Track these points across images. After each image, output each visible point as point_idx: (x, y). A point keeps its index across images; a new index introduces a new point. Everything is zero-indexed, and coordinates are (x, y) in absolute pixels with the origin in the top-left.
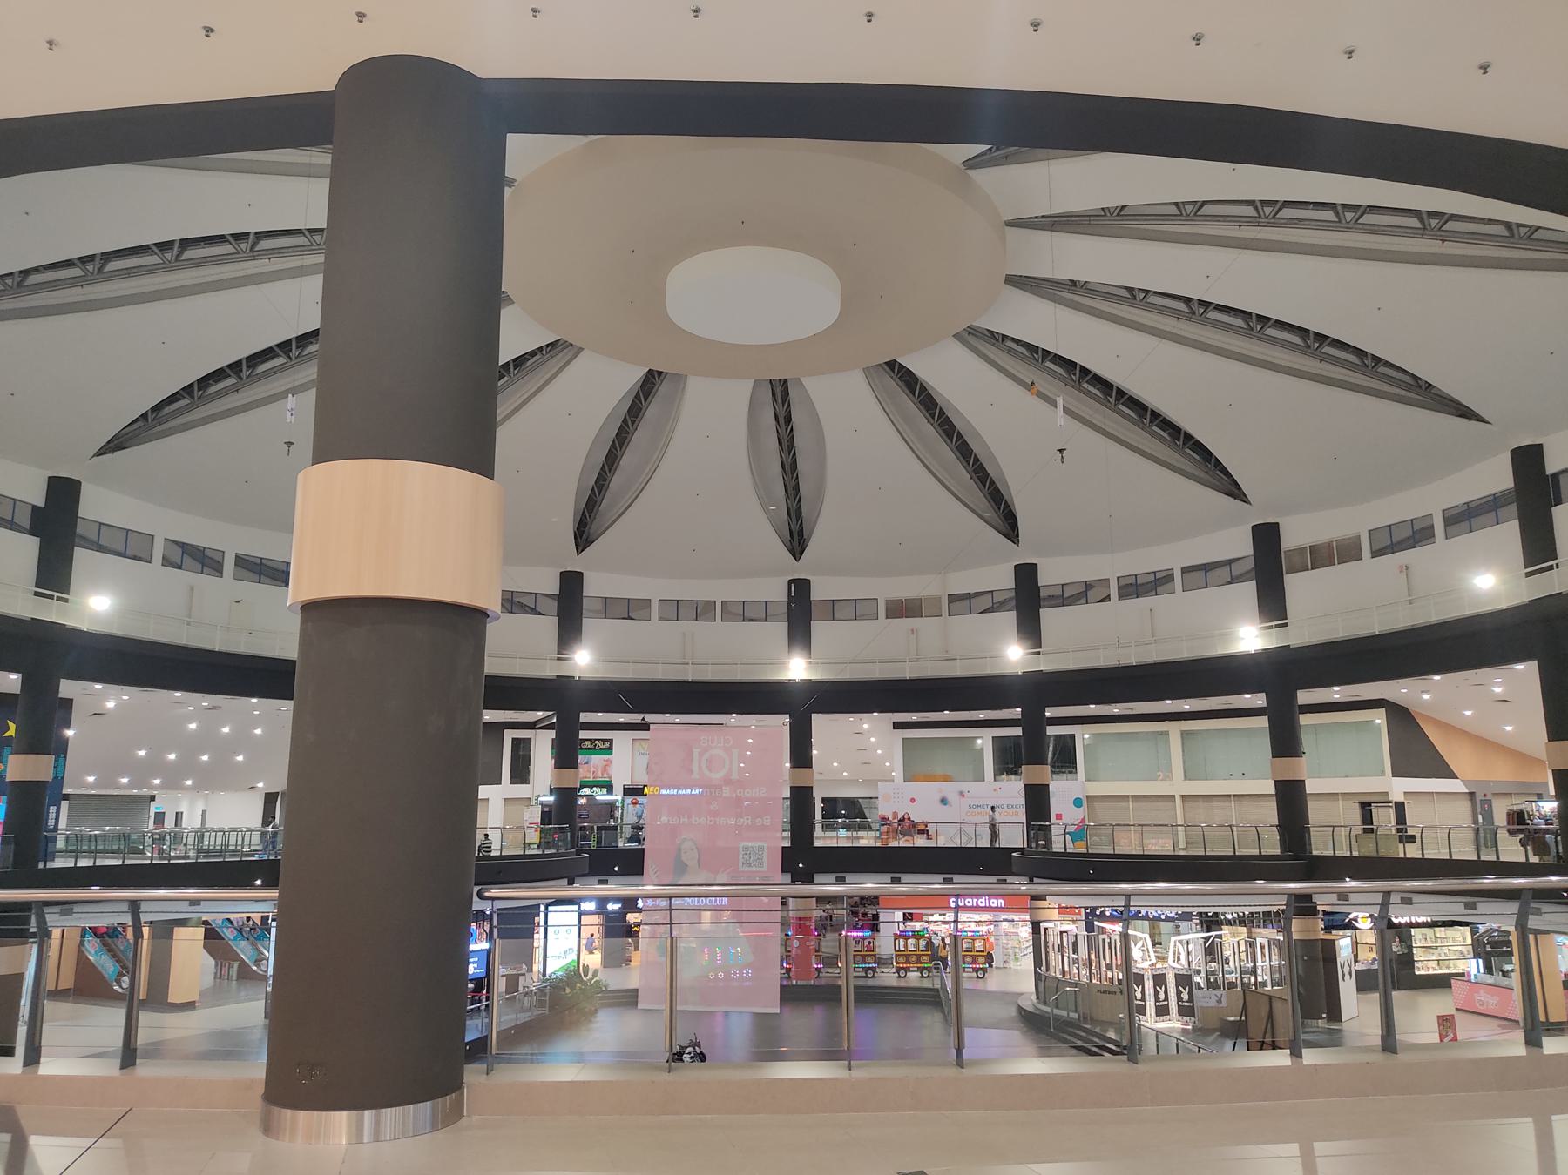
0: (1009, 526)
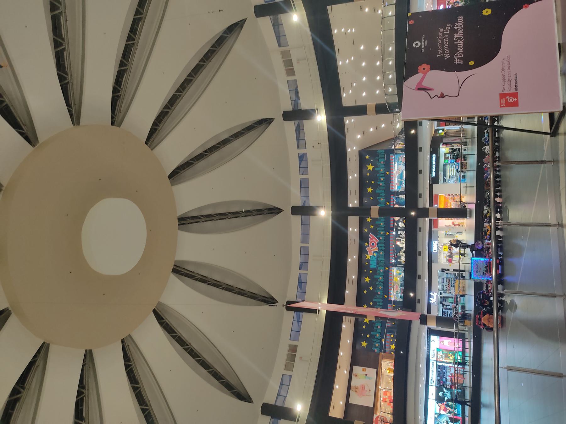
0: (266, 122)
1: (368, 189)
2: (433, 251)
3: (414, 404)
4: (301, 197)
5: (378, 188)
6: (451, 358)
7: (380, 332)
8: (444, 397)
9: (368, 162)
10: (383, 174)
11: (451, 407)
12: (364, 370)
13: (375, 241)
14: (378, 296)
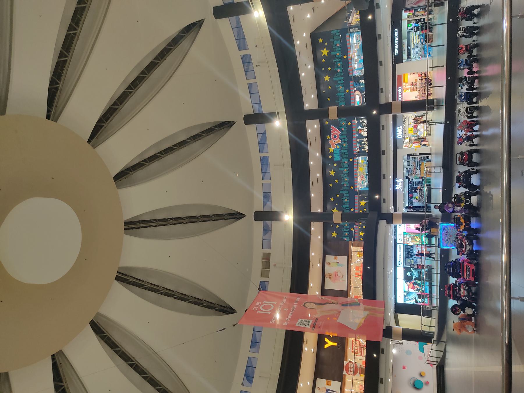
1: (322, 42)
2: (398, 137)
3: (383, 272)
4: (252, 104)
6: (418, 240)
7: (340, 51)
9: (322, 46)
10: (340, 58)
11: (419, 285)
12: (335, 258)
13: (337, 132)
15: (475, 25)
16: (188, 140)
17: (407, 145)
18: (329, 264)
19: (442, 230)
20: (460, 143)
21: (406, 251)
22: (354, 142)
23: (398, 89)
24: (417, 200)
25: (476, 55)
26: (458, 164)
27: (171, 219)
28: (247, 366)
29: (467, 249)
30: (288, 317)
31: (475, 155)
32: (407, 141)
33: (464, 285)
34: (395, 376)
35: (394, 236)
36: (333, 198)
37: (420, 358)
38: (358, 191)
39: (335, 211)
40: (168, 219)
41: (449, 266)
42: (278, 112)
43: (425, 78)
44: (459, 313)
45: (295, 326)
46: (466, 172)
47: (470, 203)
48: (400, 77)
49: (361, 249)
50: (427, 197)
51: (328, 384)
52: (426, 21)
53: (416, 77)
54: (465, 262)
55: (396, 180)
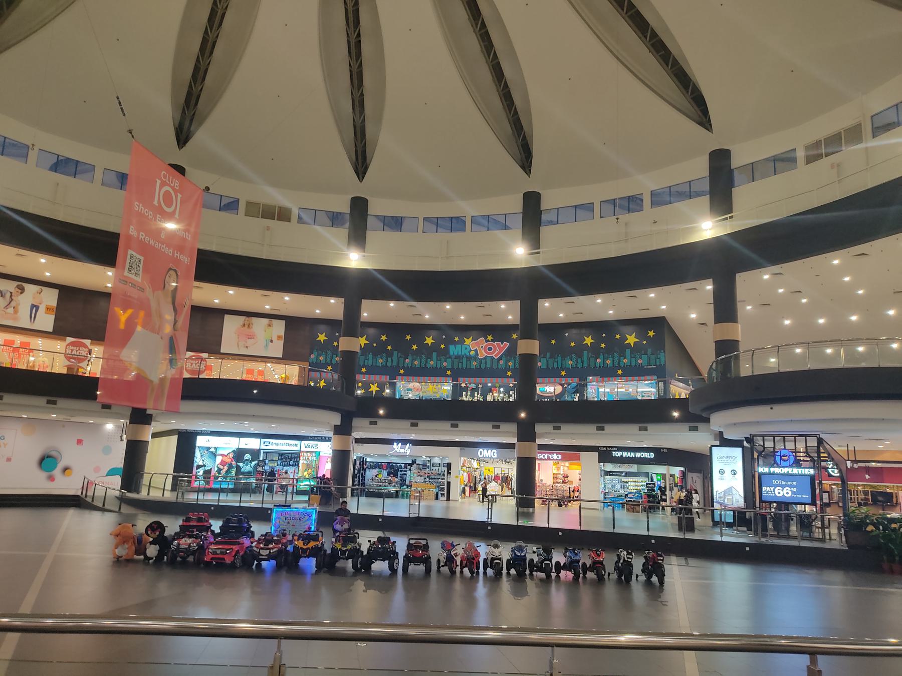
5: (593, 355)
6: (305, 474)
7: (631, 363)
8: (244, 463)
9: (642, 335)
12: (279, 337)
13: (496, 352)
14: (401, 360)
15: (634, 577)
16: (503, 82)
17: (467, 465)
18: (269, 325)
19: (304, 511)
20: (444, 546)
21: (293, 455)
22: (478, 380)
23: (557, 454)
24: (376, 476)
25: (586, 577)
26: (409, 540)
27: (359, 35)
28: (78, 162)
29: (261, 550)
30: (147, 237)
31: (422, 567)
32: (475, 464)
33: (198, 544)
34: (64, 426)
35: (314, 437)
36: (386, 337)
37: (97, 469)
38: (395, 381)
39: (363, 341)
40: (358, 29)
41: (240, 521)
42: (539, 253)
43: (572, 496)
44: (148, 535)
45: (128, 247)
46: (396, 554)
47: (340, 558)
48: (578, 458)
49: (294, 381)
50: (377, 491)
51: (48, 309)
52: (661, 503)
53: (576, 483)
54: (240, 547)
55: (408, 444)
